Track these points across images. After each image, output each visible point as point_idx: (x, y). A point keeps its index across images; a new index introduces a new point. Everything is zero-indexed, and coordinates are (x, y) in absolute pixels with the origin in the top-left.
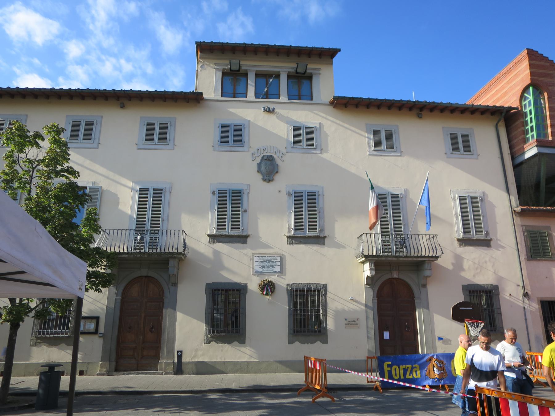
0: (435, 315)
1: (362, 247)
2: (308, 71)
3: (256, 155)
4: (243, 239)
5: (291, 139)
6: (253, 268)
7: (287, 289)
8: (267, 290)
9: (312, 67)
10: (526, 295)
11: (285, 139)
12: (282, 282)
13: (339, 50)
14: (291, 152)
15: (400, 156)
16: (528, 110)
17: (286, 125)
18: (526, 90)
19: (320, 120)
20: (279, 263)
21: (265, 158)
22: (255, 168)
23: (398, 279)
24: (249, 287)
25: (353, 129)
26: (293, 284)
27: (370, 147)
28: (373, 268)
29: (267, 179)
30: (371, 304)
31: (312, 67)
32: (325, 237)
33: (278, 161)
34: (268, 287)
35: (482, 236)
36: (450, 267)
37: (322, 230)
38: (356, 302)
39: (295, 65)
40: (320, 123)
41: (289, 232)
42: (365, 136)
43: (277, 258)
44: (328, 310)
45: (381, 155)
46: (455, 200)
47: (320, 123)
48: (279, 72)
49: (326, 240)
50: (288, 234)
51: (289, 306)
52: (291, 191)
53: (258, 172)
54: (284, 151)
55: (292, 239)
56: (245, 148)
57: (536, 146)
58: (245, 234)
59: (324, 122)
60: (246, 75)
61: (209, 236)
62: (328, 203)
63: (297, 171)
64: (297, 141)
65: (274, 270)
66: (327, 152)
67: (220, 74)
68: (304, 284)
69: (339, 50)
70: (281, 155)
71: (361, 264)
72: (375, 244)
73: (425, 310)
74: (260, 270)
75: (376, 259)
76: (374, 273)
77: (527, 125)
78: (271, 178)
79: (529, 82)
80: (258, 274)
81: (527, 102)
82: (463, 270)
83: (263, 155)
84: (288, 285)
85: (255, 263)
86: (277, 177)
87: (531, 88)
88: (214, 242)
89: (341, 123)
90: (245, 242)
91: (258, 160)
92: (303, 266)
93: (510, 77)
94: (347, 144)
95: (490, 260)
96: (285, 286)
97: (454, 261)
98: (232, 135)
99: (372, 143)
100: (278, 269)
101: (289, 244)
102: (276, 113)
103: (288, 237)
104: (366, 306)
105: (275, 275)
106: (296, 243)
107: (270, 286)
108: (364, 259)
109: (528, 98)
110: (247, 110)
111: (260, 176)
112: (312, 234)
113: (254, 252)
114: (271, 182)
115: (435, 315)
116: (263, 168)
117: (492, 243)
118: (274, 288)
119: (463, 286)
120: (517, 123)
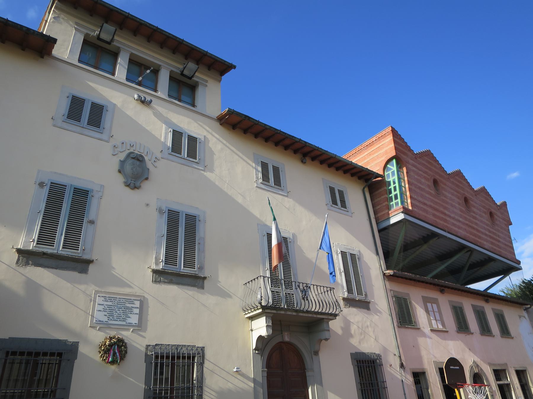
0: (328, 392)
1: (259, 293)
2: (194, 79)
3: (120, 149)
4: (82, 265)
5: (169, 143)
6: (93, 316)
7: (146, 355)
8: (115, 354)
9: (199, 76)
10: (402, 366)
11: (160, 141)
12: (139, 342)
13: (234, 67)
14: (168, 159)
15: (287, 196)
16: (391, 179)
17: (164, 126)
18: (389, 161)
19: (205, 133)
20: (137, 311)
21: (132, 156)
22: (117, 167)
23: (288, 344)
24: (82, 349)
25: (241, 155)
26: (156, 345)
27: (257, 178)
28: (270, 324)
29: (132, 185)
30: (260, 379)
31: (199, 76)
32: (205, 278)
33: (149, 165)
34: (116, 351)
35: (362, 297)
36: (340, 332)
37: (201, 268)
38: (243, 375)
39: (181, 67)
40: (205, 136)
41: (157, 263)
42: (253, 167)
43: (136, 302)
44: (205, 388)
45: (269, 191)
46: (337, 255)
47: (205, 136)
48: (160, 66)
49: (206, 282)
50: (154, 267)
51: (147, 382)
52: (164, 208)
53: (120, 171)
54: (159, 155)
55: (160, 275)
56: (104, 136)
57: (402, 212)
58: (86, 257)
59: (209, 136)
60: (115, 55)
61: (19, 251)
62: (210, 233)
63: (171, 185)
64: (176, 148)
65: (129, 320)
66: (212, 171)
67: (81, 38)
68: (173, 346)
69: (234, 67)
70: (154, 159)
71: (248, 320)
72: (263, 292)
73: (319, 386)
74: (105, 319)
75: (275, 312)
76: (271, 331)
77: (390, 192)
78: (138, 184)
79: (393, 153)
80: (102, 326)
81: (390, 172)
82: (352, 336)
83: (129, 151)
84: (148, 346)
85: (97, 307)
86: (146, 185)
87: (394, 160)
88: (27, 264)
89: (228, 144)
90: (84, 271)
91: (122, 157)
92: (172, 319)
93: (373, 149)
94: (233, 168)
95: (370, 325)
96: (143, 349)
97: (342, 325)
98: (87, 114)
99: (260, 175)
100: (134, 319)
101: (155, 281)
102: (152, 108)
103: (155, 272)
104: (254, 381)
105: (128, 330)
106: (165, 282)
107: (119, 347)
108: (260, 310)
109: (391, 169)
110: (115, 92)
111: (120, 179)
112: (188, 271)
113: (97, 289)
114: (136, 190)
115: (328, 392)
116: (128, 168)
117: (371, 306)
118: (126, 352)
119: (351, 354)
120: (380, 190)
